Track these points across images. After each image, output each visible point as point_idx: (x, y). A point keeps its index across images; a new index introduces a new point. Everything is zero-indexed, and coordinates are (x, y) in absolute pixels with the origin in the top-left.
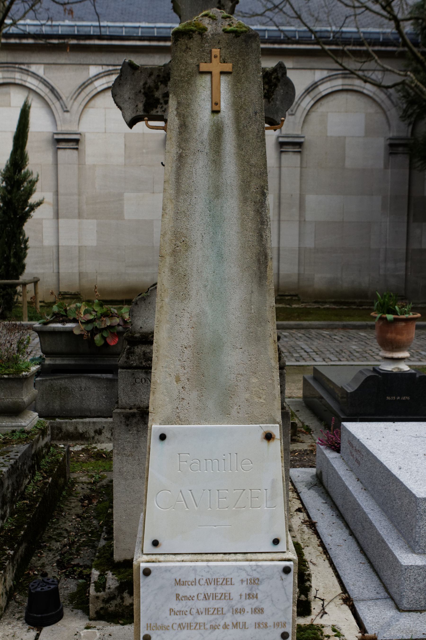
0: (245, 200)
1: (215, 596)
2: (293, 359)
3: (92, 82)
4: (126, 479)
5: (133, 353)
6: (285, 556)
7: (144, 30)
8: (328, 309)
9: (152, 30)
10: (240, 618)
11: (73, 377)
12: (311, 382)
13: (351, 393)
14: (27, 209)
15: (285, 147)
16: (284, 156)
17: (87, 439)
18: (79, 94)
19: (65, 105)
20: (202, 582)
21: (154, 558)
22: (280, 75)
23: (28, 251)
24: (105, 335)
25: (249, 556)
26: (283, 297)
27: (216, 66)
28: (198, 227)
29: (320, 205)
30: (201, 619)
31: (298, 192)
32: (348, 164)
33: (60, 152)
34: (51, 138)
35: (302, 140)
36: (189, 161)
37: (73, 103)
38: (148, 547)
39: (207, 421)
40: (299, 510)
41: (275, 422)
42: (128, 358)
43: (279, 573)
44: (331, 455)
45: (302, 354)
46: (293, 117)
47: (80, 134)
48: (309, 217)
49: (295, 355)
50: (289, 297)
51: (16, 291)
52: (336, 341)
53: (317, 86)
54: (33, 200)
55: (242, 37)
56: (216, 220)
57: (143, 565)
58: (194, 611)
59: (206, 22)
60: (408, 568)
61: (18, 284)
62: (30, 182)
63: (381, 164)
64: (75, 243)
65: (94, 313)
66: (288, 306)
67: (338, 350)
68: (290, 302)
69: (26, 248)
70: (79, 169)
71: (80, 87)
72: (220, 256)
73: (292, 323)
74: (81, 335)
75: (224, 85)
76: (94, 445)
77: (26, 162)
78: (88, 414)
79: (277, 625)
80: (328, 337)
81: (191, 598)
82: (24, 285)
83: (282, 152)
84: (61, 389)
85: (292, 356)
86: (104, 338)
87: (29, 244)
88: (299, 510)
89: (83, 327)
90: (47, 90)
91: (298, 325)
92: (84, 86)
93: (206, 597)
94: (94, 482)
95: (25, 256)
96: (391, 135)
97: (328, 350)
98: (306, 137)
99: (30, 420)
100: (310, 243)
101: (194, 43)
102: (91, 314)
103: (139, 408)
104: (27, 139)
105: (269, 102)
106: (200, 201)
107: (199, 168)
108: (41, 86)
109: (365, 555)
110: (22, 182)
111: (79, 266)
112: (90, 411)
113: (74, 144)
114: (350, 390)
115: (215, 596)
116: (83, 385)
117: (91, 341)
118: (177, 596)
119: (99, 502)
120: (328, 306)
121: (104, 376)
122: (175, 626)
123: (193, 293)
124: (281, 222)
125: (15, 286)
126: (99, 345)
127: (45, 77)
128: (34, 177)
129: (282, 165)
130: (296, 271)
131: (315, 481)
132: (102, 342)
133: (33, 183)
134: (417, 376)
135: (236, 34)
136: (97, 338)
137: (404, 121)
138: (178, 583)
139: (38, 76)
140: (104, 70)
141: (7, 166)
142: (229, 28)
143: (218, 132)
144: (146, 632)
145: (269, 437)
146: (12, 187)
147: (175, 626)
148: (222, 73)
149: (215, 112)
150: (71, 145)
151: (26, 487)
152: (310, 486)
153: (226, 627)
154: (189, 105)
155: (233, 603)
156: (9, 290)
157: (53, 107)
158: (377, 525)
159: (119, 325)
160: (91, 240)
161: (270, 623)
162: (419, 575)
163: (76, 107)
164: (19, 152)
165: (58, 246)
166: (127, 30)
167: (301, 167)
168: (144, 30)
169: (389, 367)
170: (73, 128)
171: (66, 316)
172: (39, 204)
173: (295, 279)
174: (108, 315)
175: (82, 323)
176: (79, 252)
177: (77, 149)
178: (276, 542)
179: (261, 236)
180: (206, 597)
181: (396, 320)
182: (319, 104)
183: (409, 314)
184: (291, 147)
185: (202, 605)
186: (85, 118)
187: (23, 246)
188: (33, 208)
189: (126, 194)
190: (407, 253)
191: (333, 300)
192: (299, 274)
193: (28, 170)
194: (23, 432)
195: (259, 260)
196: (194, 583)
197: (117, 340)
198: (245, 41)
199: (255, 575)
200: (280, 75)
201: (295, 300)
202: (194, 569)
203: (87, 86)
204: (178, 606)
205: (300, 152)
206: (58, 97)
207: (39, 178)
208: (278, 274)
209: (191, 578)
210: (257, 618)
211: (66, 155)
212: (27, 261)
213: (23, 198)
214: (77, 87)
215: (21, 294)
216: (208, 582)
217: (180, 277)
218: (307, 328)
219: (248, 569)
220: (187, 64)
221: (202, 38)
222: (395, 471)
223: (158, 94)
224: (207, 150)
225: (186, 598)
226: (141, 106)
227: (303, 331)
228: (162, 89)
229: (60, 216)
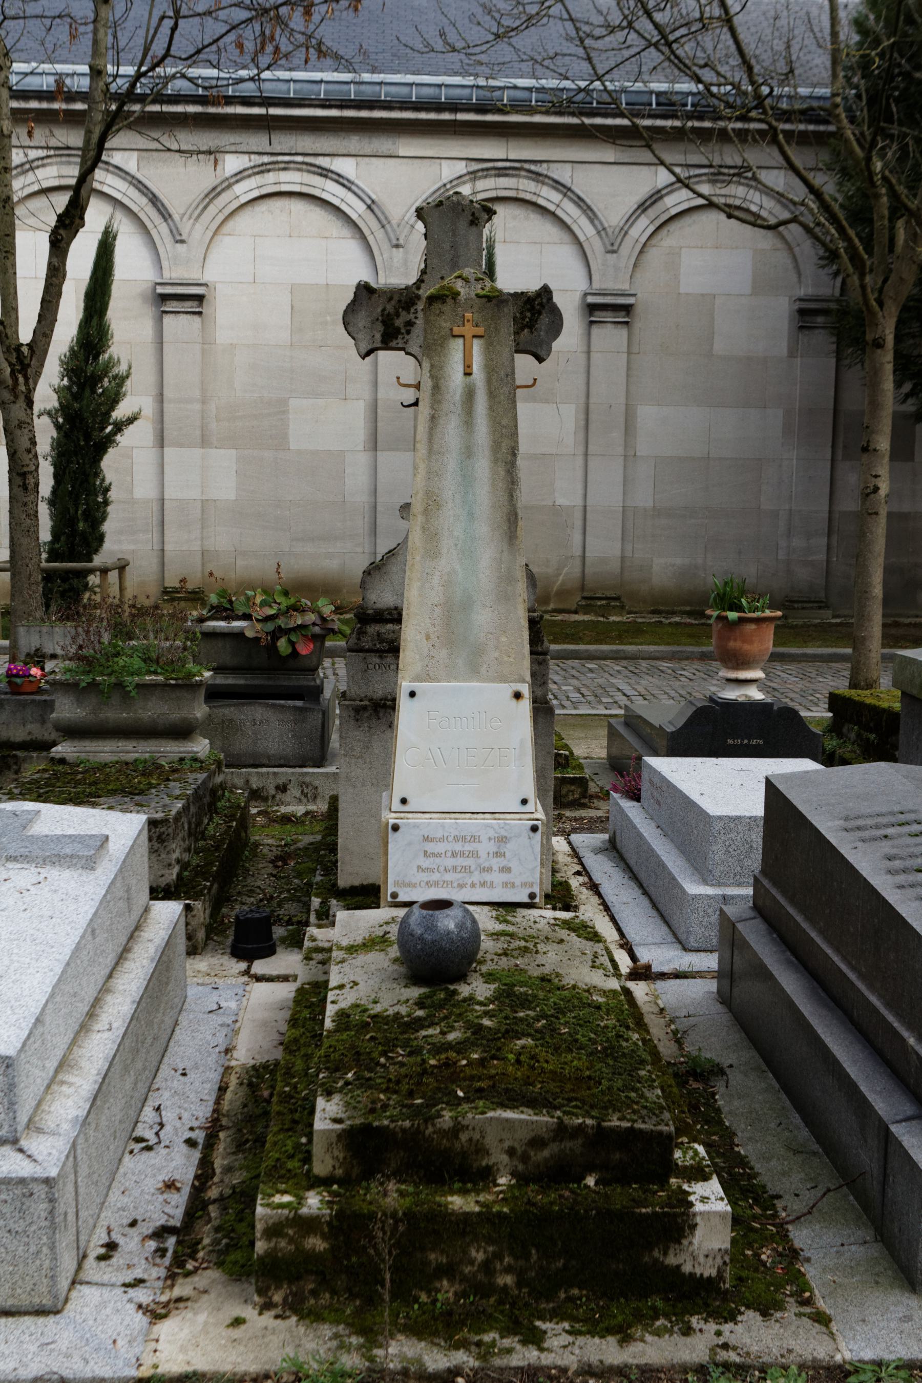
0: (496, 461)
1: (462, 854)
2: (601, 707)
3: (229, 186)
4: (354, 787)
5: (365, 633)
6: (532, 816)
7: (331, 87)
8: (678, 624)
9: (345, 87)
10: (488, 877)
11: (243, 704)
12: (622, 730)
13: (672, 733)
14: (109, 428)
15: (597, 313)
16: (595, 330)
17: (265, 799)
18: (205, 208)
19: (177, 229)
20: (450, 839)
21: (402, 815)
22: (544, 301)
23: (109, 509)
24: (294, 639)
25: (497, 816)
26: (592, 602)
27: (468, 330)
28: (449, 486)
29: (669, 426)
30: (448, 877)
31: (623, 400)
32: (719, 347)
33: (167, 319)
34: (150, 291)
35: (631, 301)
36: (441, 422)
37: (194, 225)
38: (396, 805)
39: (456, 679)
40: (578, 873)
41: (524, 681)
42: (359, 639)
43: (526, 832)
44: (628, 805)
45: (617, 698)
46: (615, 255)
47: (206, 285)
48: (643, 447)
49: (604, 700)
50: (604, 602)
51: (87, 584)
52: (682, 679)
53: (661, 198)
54: (120, 412)
55: (494, 301)
56: (467, 480)
57: (392, 822)
58: (441, 869)
59: (459, 286)
60: (695, 897)
61: (92, 571)
62: (115, 377)
63: (782, 348)
64: (194, 494)
65: (275, 606)
66: (601, 619)
67: (683, 693)
68: (604, 611)
69: (106, 503)
70: (203, 352)
71: (206, 196)
72: (471, 516)
73: (605, 647)
74: (257, 640)
75: (477, 347)
76: (275, 808)
77: (108, 340)
78: (265, 761)
79: (524, 885)
80: (670, 671)
81: (438, 855)
82: (104, 571)
83: (592, 322)
84: (223, 722)
85: (600, 702)
86: (292, 644)
87: (112, 495)
88: (578, 873)
89: (259, 626)
90: (144, 201)
91: (617, 652)
92: (214, 193)
93: (454, 855)
94: (286, 845)
95: (104, 518)
96: (802, 293)
97: (665, 693)
98: (639, 295)
99: (201, 746)
100: (643, 498)
101: (447, 308)
102: (271, 607)
103: (371, 700)
104: (109, 297)
105: (532, 332)
106: (451, 462)
107: (451, 428)
108: (133, 193)
109: (657, 910)
110: (101, 379)
111: (202, 539)
112: (269, 757)
113: (195, 303)
114: (670, 729)
115: (462, 854)
116: (258, 717)
117: (272, 647)
118: (425, 852)
119: (297, 863)
120: (677, 619)
121: (290, 703)
122: (423, 884)
123: (445, 551)
124: (589, 458)
125: (83, 574)
126: (284, 654)
127: (139, 176)
128: (122, 368)
129: (593, 349)
130: (618, 553)
131: (607, 845)
132: (290, 650)
133: (121, 380)
134: (775, 708)
135: (489, 298)
136: (282, 643)
137: (823, 267)
138: (427, 839)
139: (127, 173)
140: (252, 164)
141: (71, 349)
142: (482, 293)
143: (470, 394)
144: (394, 890)
145: (518, 696)
146: (82, 387)
147: (423, 884)
148: (474, 336)
149: (468, 374)
150: (188, 306)
151: (206, 829)
152: (598, 851)
153: (473, 885)
154: (441, 368)
155: (481, 861)
156: (75, 582)
157: (154, 233)
158: (670, 865)
159: (314, 624)
160: (225, 488)
161: (518, 883)
162: (710, 907)
163: (197, 233)
164: (94, 322)
165: (162, 500)
166: (298, 86)
167: (629, 353)
168: (331, 87)
169: (732, 694)
170: (193, 275)
171: (232, 610)
172: (131, 420)
173: (615, 566)
174: (296, 608)
175: (258, 620)
176: (203, 511)
177: (200, 313)
178: (524, 802)
179: (512, 496)
180: (454, 855)
181: (741, 620)
182: (664, 232)
183: (763, 612)
184: (609, 313)
185: (450, 862)
186: (213, 256)
187: (100, 500)
188: (119, 427)
189: (292, 402)
190: (830, 519)
191: (688, 608)
192: (623, 558)
193: (110, 357)
194: (195, 760)
195: (509, 520)
196: (442, 840)
197: (312, 646)
198: (497, 306)
199: (503, 833)
200: (544, 301)
201: (614, 607)
202: (443, 826)
203: (219, 194)
204: (426, 863)
205: (627, 323)
206: (165, 215)
207: (132, 370)
208: (584, 557)
209: (439, 835)
210: (505, 877)
211: (178, 326)
212: (107, 527)
213: (103, 409)
214: (202, 196)
215: (97, 590)
216: (456, 839)
217: (432, 536)
218: (633, 657)
219: (496, 827)
220: (440, 327)
221: (455, 303)
222: (694, 797)
223: (399, 322)
224: (459, 411)
225: (434, 855)
226: (378, 336)
227: (625, 663)
228: (404, 316)
229: (166, 442)
